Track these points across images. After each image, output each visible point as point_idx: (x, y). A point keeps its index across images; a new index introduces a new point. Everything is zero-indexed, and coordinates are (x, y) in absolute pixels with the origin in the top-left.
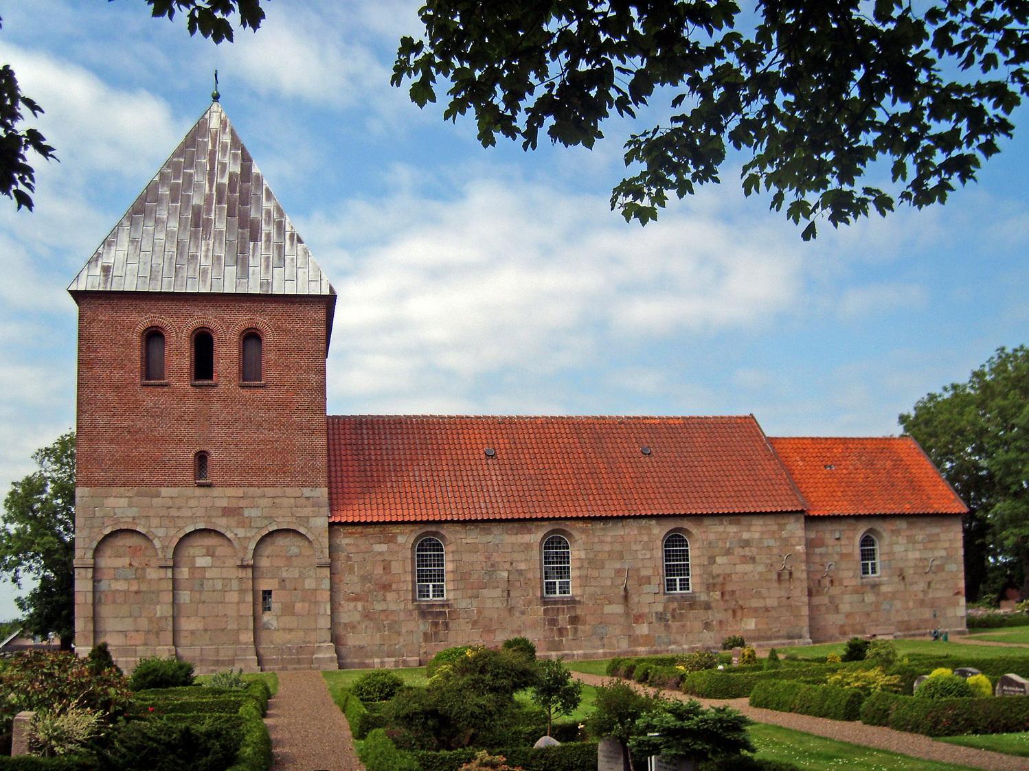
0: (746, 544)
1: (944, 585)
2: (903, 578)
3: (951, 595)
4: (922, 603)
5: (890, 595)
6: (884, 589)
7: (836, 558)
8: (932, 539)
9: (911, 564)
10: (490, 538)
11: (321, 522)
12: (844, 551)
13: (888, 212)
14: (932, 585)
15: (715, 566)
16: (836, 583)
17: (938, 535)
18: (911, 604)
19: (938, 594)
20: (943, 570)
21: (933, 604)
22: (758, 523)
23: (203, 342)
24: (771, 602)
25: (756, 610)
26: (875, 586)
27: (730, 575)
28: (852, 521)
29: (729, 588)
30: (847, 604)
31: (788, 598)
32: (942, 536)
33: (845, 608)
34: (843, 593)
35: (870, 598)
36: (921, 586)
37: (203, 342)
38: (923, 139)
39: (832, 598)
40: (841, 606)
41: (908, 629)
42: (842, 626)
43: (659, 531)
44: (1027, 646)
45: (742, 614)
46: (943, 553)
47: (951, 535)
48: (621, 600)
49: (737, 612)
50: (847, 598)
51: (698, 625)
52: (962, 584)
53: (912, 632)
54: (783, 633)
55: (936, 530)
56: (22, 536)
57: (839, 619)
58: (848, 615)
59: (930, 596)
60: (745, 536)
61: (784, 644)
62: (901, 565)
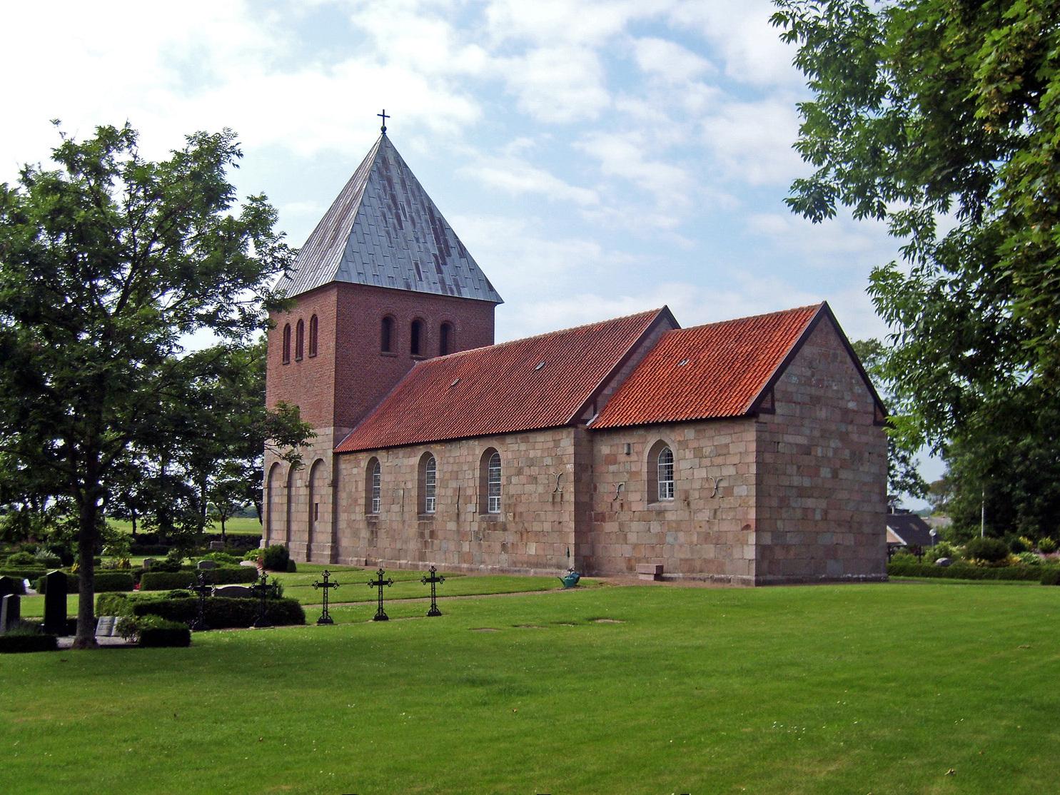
0: (531, 463)
1: (732, 514)
2: (688, 504)
3: (740, 528)
4: (706, 538)
5: (674, 525)
6: (670, 516)
7: (626, 476)
8: (722, 451)
9: (697, 485)
10: (397, 461)
11: (330, 453)
12: (633, 469)
13: (811, 89)
14: (718, 513)
15: (511, 486)
16: (626, 507)
17: (727, 446)
18: (695, 539)
19: (725, 527)
20: (731, 494)
21: (717, 540)
22: (540, 438)
23: (416, 326)
24: (547, 527)
25: (537, 533)
26: (661, 513)
27: (520, 496)
28: (642, 432)
29: (519, 509)
30: (635, 531)
31: (560, 523)
32: (732, 449)
33: (632, 538)
34: (631, 520)
35: (655, 527)
36: (705, 515)
37: (416, 326)
38: (118, 241)
39: (621, 525)
40: (629, 536)
41: (692, 570)
42: (629, 560)
43: (478, 449)
44: (1058, 657)
45: (528, 538)
46: (731, 471)
47: (742, 448)
48: (455, 518)
49: (523, 533)
50: (635, 526)
51: (498, 547)
52: (752, 515)
53: (694, 575)
54: (554, 561)
55: (724, 440)
56: (779, 554)
57: (627, 551)
58: (635, 546)
59: (716, 528)
60: (532, 454)
61: (552, 573)
62: (687, 487)
